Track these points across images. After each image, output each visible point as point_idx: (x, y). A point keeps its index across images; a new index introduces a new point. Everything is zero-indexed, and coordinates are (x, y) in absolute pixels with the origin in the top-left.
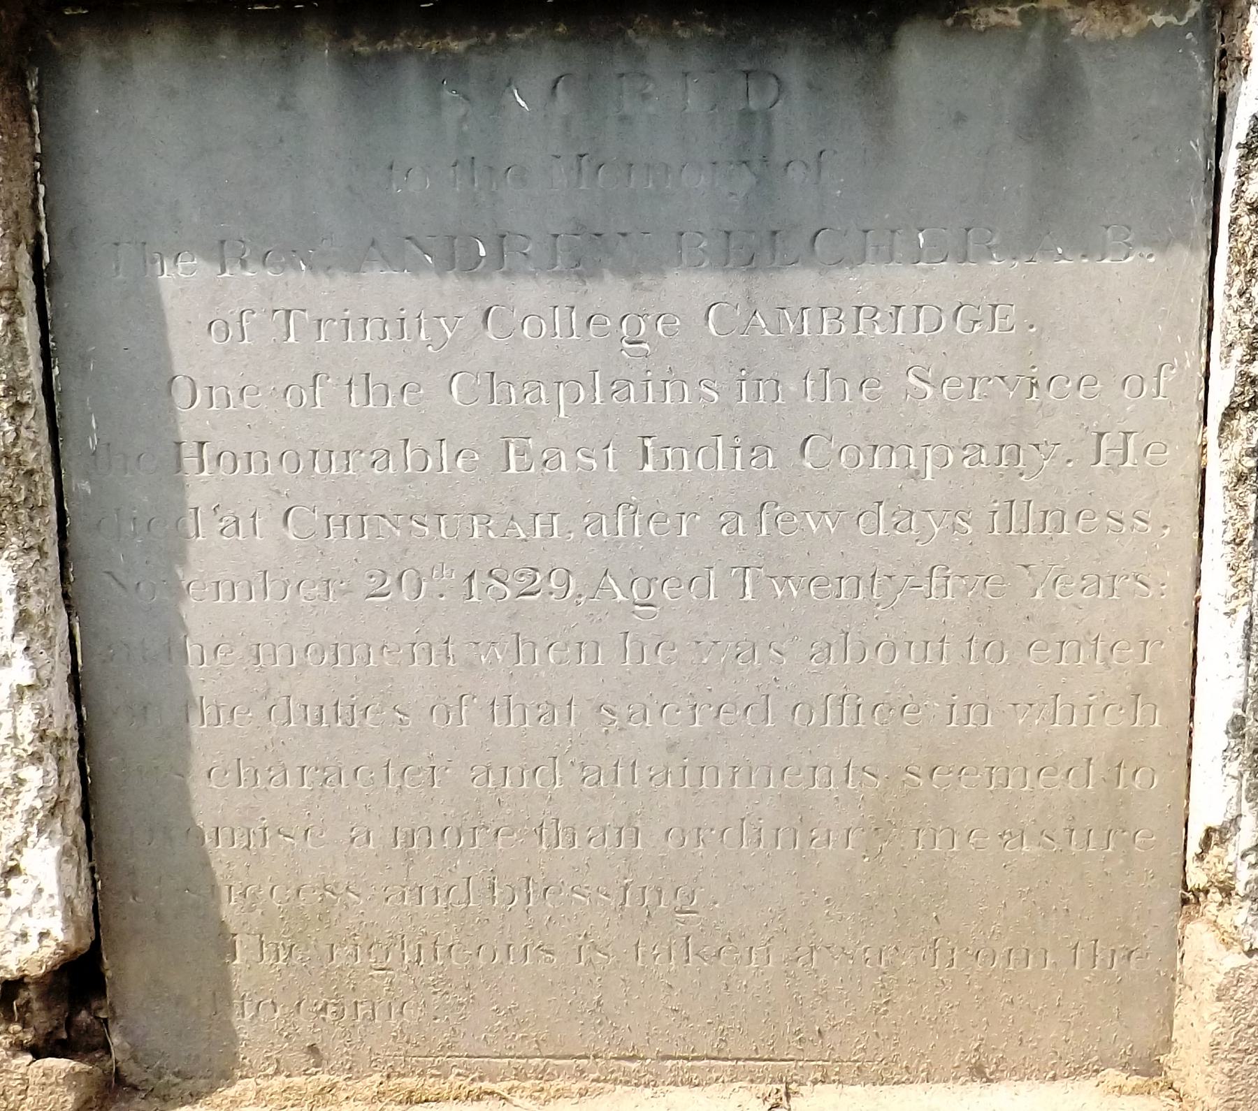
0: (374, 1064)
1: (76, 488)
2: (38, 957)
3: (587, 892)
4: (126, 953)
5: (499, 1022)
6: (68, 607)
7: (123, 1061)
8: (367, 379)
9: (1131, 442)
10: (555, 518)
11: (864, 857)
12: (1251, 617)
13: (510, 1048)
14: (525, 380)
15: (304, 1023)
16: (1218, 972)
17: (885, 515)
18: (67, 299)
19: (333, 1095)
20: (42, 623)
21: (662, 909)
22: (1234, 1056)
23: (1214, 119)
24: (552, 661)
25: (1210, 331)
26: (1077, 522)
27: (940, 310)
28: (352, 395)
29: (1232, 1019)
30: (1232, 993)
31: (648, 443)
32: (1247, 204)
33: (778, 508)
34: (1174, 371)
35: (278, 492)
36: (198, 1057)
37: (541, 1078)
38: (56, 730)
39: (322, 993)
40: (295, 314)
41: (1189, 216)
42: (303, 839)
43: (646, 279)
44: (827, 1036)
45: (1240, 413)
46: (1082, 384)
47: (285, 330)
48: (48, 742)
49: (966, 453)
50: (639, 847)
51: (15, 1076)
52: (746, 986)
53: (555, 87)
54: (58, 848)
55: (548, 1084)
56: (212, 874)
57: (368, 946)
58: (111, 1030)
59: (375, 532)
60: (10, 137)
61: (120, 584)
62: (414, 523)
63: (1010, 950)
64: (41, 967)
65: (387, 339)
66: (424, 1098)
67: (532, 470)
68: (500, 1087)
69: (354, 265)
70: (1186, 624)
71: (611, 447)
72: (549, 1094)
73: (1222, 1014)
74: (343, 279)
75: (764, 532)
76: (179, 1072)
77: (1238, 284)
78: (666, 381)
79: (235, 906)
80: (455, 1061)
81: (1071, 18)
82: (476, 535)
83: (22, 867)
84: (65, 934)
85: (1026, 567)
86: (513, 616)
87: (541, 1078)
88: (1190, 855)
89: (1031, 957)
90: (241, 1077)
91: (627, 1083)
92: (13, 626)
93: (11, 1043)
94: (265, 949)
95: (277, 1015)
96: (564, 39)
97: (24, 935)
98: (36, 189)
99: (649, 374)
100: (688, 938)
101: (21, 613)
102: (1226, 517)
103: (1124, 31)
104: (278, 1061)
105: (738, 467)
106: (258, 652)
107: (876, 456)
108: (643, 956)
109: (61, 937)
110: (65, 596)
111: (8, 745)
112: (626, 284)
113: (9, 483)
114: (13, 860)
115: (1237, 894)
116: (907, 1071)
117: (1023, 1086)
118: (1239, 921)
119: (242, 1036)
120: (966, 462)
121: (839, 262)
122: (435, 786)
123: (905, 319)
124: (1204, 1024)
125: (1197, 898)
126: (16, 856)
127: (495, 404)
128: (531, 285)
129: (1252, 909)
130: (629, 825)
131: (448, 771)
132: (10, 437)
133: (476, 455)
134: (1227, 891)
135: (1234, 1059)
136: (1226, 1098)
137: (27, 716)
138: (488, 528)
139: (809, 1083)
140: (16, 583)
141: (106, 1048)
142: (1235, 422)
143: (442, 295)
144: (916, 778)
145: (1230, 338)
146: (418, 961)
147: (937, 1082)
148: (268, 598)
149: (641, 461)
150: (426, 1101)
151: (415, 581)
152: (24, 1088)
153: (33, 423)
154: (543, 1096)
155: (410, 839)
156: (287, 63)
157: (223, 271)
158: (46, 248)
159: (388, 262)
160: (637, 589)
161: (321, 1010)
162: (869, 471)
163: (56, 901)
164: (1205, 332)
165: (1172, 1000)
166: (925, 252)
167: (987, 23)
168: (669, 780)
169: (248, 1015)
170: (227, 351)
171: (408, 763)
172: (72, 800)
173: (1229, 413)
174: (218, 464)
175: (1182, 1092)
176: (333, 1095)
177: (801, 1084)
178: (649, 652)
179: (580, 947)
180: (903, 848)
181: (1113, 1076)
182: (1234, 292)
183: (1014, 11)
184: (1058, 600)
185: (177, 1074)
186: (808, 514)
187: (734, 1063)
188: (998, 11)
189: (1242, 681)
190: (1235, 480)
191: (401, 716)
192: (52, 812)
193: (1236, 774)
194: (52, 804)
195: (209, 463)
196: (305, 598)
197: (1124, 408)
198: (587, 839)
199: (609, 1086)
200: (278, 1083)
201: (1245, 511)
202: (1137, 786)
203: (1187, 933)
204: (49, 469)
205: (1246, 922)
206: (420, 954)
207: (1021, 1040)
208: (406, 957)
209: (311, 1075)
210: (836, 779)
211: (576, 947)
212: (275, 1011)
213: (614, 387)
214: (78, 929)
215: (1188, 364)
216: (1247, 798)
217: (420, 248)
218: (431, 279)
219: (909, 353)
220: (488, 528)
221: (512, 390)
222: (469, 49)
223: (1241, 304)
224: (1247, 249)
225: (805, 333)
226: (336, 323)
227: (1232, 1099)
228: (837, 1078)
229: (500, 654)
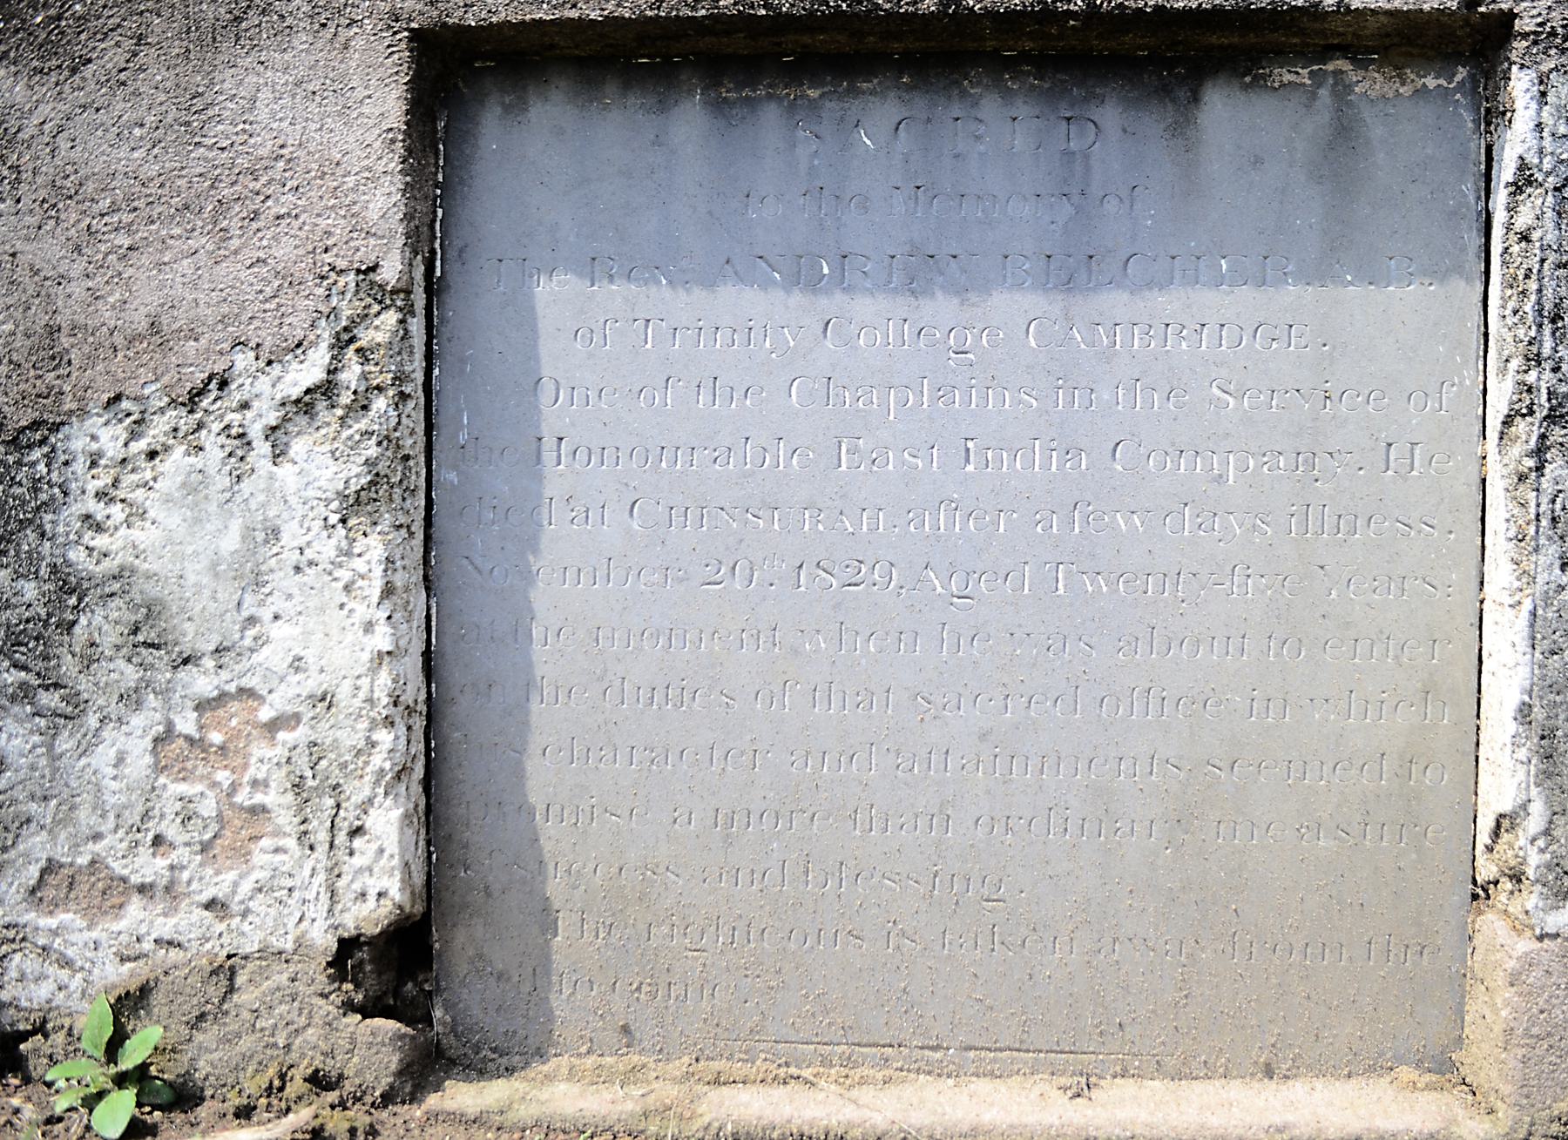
0: (684, 1046)
1: (445, 479)
2: (375, 916)
3: (897, 877)
4: (454, 926)
5: (808, 1007)
6: (428, 589)
7: (444, 1034)
8: (714, 383)
9: (1417, 451)
10: (881, 513)
11: (1167, 848)
12: (1535, 609)
13: (817, 1034)
14: (859, 385)
15: (618, 1003)
16: (1510, 957)
17: (1190, 516)
18: (454, 307)
19: (643, 1074)
20: (404, 595)
21: (969, 898)
22: (1527, 1041)
23: (1483, 167)
24: (872, 649)
25: (1486, 352)
26: (1369, 526)
27: (1241, 328)
28: (700, 397)
29: (1524, 1004)
30: (1524, 977)
31: (970, 444)
32: (1516, 233)
33: (1090, 508)
34: (1455, 389)
35: (626, 484)
36: (515, 1032)
37: (845, 1066)
38: (407, 698)
39: (637, 974)
40: (654, 323)
41: (1463, 250)
42: (628, 819)
43: (973, 297)
44: (1128, 1029)
45: (1519, 418)
46: (1372, 397)
47: (644, 337)
48: (401, 708)
49: (1265, 459)
50: (949, 834)
51: (343, 1035)
52: (1049, 977)
53: (897, 129)
54: (401, 810)
55: (853, 1072)
56: (540, 849)
57: (683, 927)
58: (434, 1002)
59: (714, 523)
60: (419, 163)
61: (476, 568)
62: (750, 516)
63: (1307, 944)
64: (377, 925)
65: (735, 347)
66: (731, 1080)
67: (862, 468)
68: (807, 1073)
69: (710, 284)
70: (1472, 625)
71: (936, 448)
72: (853, 1079)
73: (1516, 999)
74: (698, 293)
75: (1077, 530)
76: (495, 1048)
77: (1511, 305)
78: (988, 388)
79: (559, 884)
80: (762, 1046)
81: (1355, 79)
82: (807, 527)
83: (367, 826)
84: (402, 894)
85: (1322, 567)
86: (837, 606)
87: (845, 1066)
88: (1480, 847)
89: (1327, 950)
90: (555, 1055)
91: (929, 1073)
92: (379, 594)
93: (343, 1001)
94: (585, 927)
95: (593, 993)
96: (910, 88)
97: (363, 895)
98: (435, 212)
99: (973, 381)
100: (994, 926)
101: (387, 583)
102: (1508, 516)
103: (1401, 91)
104: (591, 1040)
105: (1054, 468)
106: (598, 636)
107: (1182, 460)
108: (950, 943)
109: (398, 897)
110: (426, 578)
111: (364, 708)
112: (956, 301)
113: (388, 463)
114: (358, 819)
115: (1528, 879)
116: (1205, 1066)
117: (1319, 1084)
118: (1530, 906)
119: (558, 1013)
120: (1265, 468)
121: (1148, 285)
122: (756, 769)
123: (1208, 335)
124: (1496, 1012)
125: (1485, 890)
126: (362, 816)
127: (830, 406)
128: (868, 300)
129: (1542, 894)
130: (941, 812)
131: (769, 755)
132: (393, 421)
133: (811, 453)
134: (1517, 877)
135: (1527, 1045)
136: (1520, 1084)
137: (384, 678)
138: (819, 521)
139: (1108, 1077)
140: (386, 555)
141: (429, 1021)
142: (1513, 429)
143: (787, 308)
144: (1218, 771)
145: (1506, 353)
146: (732, 943)
147: (1234, 1078)
148: (610, 585)
149: (963, 461)
150: (734, 1082)
151: (748, 571)
152: (352, 1047)
153: (413, 414)
154: (848, 1082)
155: (729, 821)
156: (663, 106)
157: (592, 285)
158: (438, 263)
159: (740, 278)
160: (956, 582)
161: (636, 989)
162: (1175, 475)
163: (396, 861)
164: (1482, 354)
165: (1463, 997)
166: (1227, 277)
167: (1281, 81)
168: (980, 769)
169: (566, 992)
170: (590, 355)
171: (731, 746)
172: (417, 770)
173: (1508, 422)
174: (574, 458)
175: (1475, 1085)
176: (643, 1074)
177: (1101, 1078)
178: (965, 641)
179: (889, 933)
180: (1204, 841)
181: (1406, 1073)
182: (1508, 312)
183: (1305, 72)
184: (1351, 599)
185: (494, 1050)
186: (1118, 514)
187: (1035, 1055)
188: (1289, 71)
189: (1528, 670)
190: (1516, 480)
191: (728, 700)
192: (398, 777)
193: (1525, 760)
194: (400, 768)
195: (566, 456)
196: (645, 584)
197: (1410, 421)
198: (899, 826)
199: (913, 1076)
200: (590, 1061)
201: (1526, 508)
202: (1427, 782)
203: (1477, 927)
204: (422, 459)
205: (1537, 907)
206: (733, 935)
207: (1317, 1036)
208: (721, 939)
209: (622, 1055)
210: (1141, 770)
211: (885, 933)
212: (592, 990)
213: (941, 393)
214: (413, 893)
215: (1468, 382)
216: (1535, 783)
217: (770, 266)
218: (778, 295)
219: (1213, 367)
220: (819, 521)
221: (847, 394)
222: (821, 96)
223: (1516, 321)
224: (1518, 273)
225: (1118, 347)
226: (690, 332)
227: (1526, 1085)
228: (1136, 1071)
229: (825, 642)
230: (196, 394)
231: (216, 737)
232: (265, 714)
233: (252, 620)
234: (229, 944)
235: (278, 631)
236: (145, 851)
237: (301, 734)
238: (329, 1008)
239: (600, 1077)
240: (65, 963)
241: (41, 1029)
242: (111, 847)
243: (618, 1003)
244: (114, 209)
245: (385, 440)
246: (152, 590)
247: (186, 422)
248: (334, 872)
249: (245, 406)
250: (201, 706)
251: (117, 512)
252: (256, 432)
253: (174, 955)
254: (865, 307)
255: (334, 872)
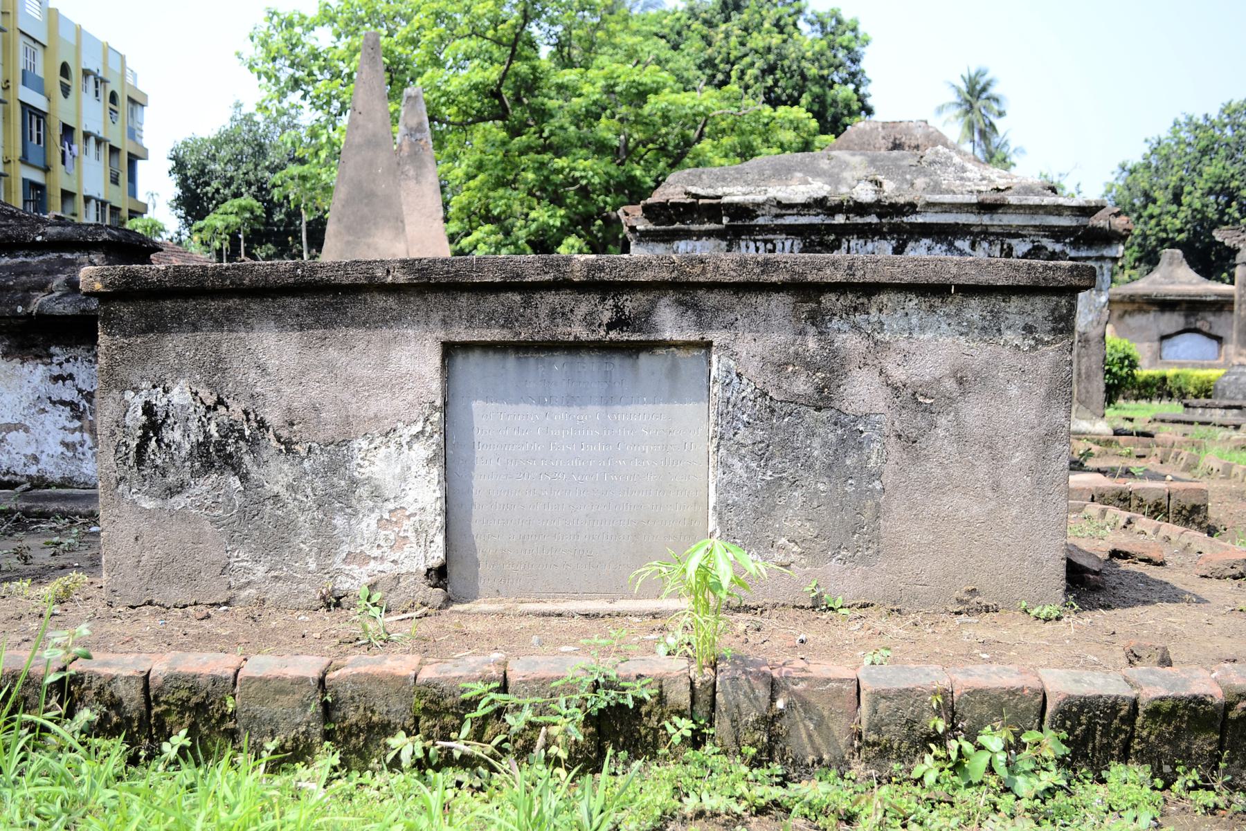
18: (450, 408)
69: (517, 403)
230: (388, 433)
231: (394, 519)
232: (407, 513)
233: (404, 490)
234: (398, 571)
235: (410, 492)
236: (375, 549)
237: (417, 518)
238: (424, 586)
239: (492, 602)
240: (354, 578)
241: (346, 595)
242: (366, 548)
243: (496, 585)
244: (364, 386)
245: (438, 445)
246: (377, 483)
247: (385, 440)
248: (426, 552)
249: (401, 436)
250: (390, 512)
251: (367, 463)
252: (404, 443)
253: (383, 575)
254: (556, 409)
255: (426, 552)
